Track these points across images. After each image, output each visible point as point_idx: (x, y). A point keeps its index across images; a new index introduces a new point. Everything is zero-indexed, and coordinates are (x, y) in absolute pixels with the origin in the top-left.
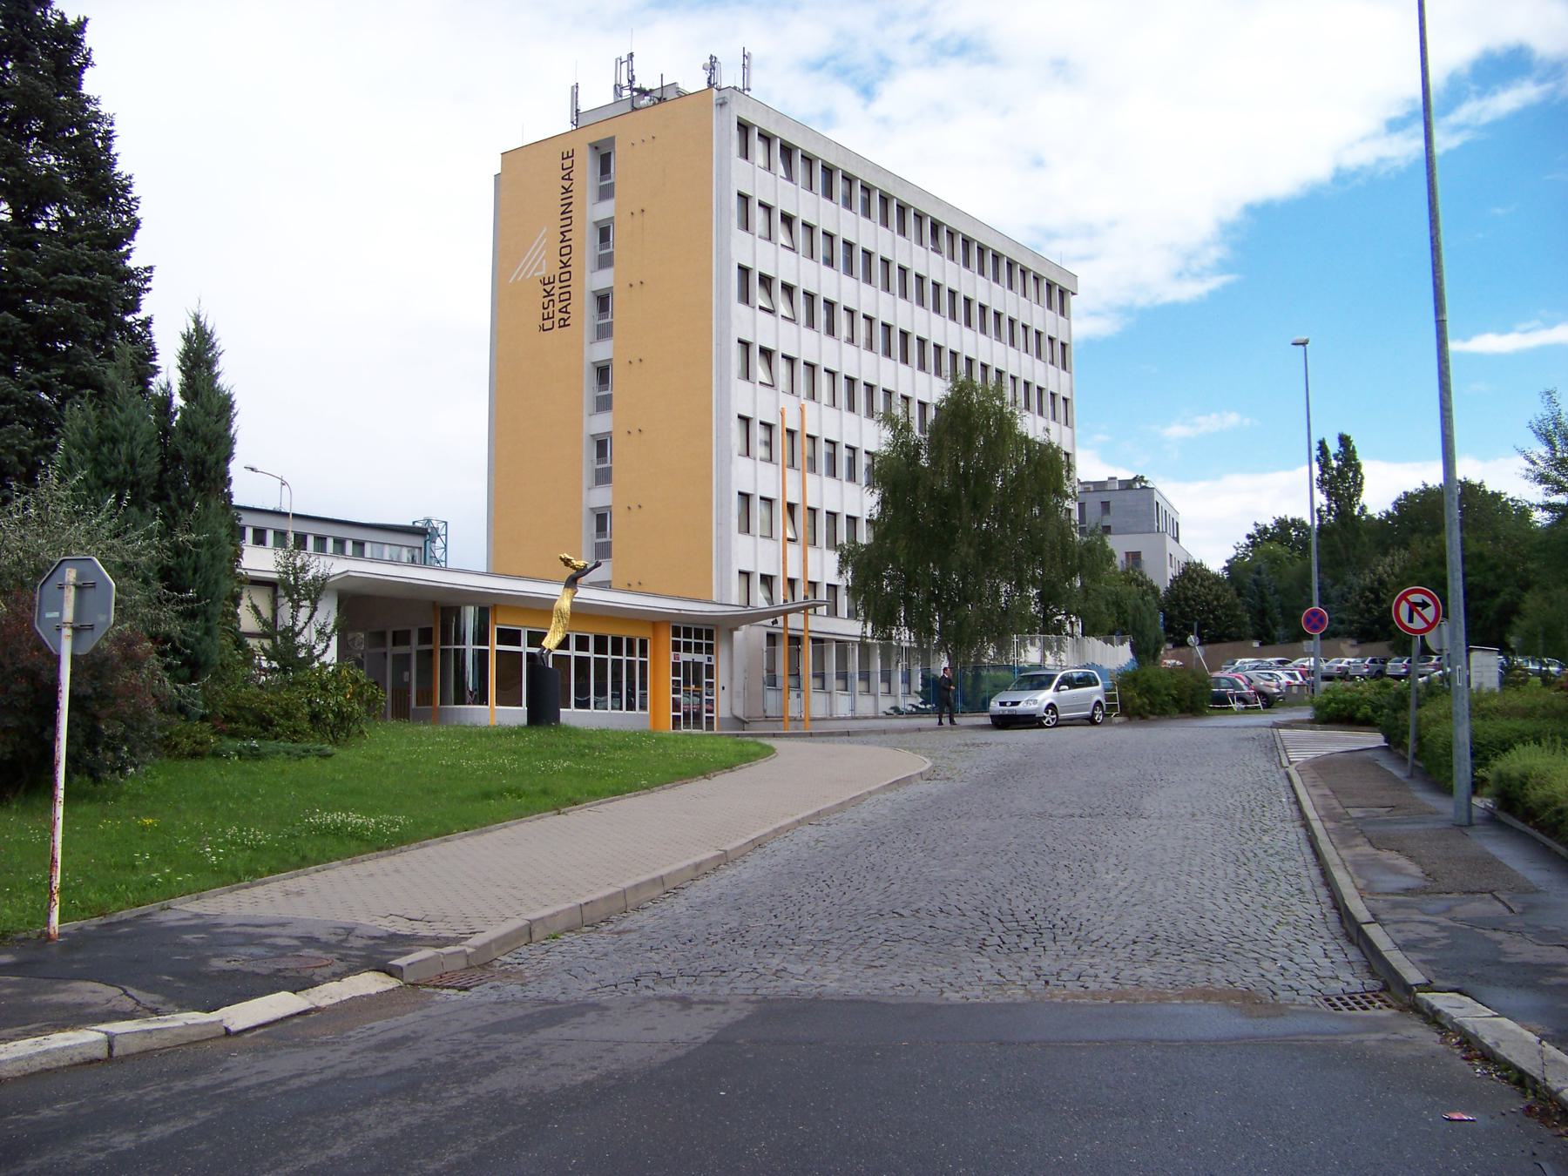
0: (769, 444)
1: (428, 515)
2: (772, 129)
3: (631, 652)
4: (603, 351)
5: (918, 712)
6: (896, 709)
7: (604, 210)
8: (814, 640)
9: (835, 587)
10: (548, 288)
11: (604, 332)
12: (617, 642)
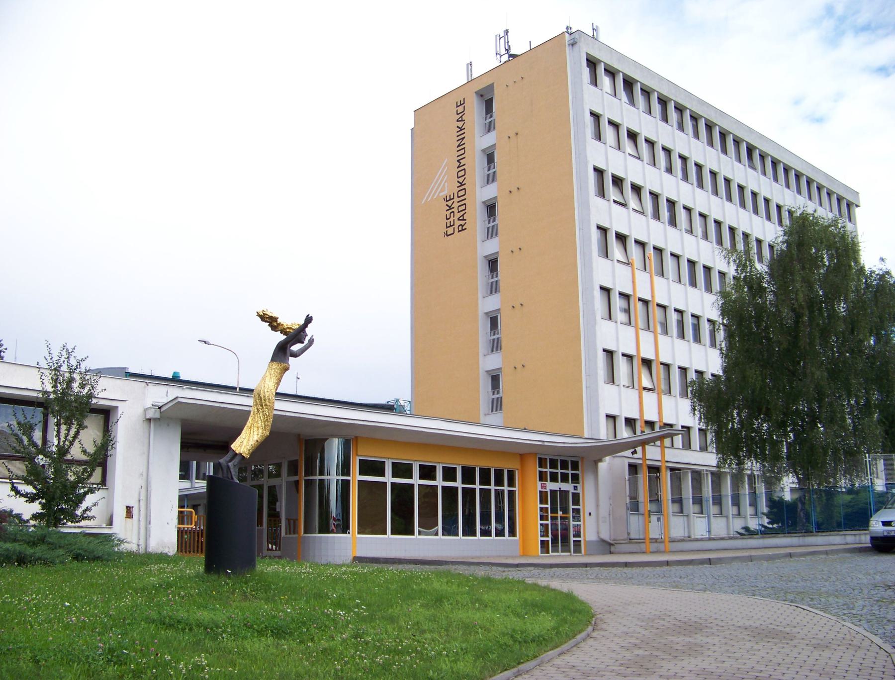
0: (627, 311)
1: (397, 397)
2: (616, 65)
3: (499, 482)
4: (491, 247)
5: (766, 532)
6: (747, 529)
7: (489, 140)
8: (672, 469)
9: (688, 428)
10: (449, 203)
11: (492, 232)
12: (485, 473)
